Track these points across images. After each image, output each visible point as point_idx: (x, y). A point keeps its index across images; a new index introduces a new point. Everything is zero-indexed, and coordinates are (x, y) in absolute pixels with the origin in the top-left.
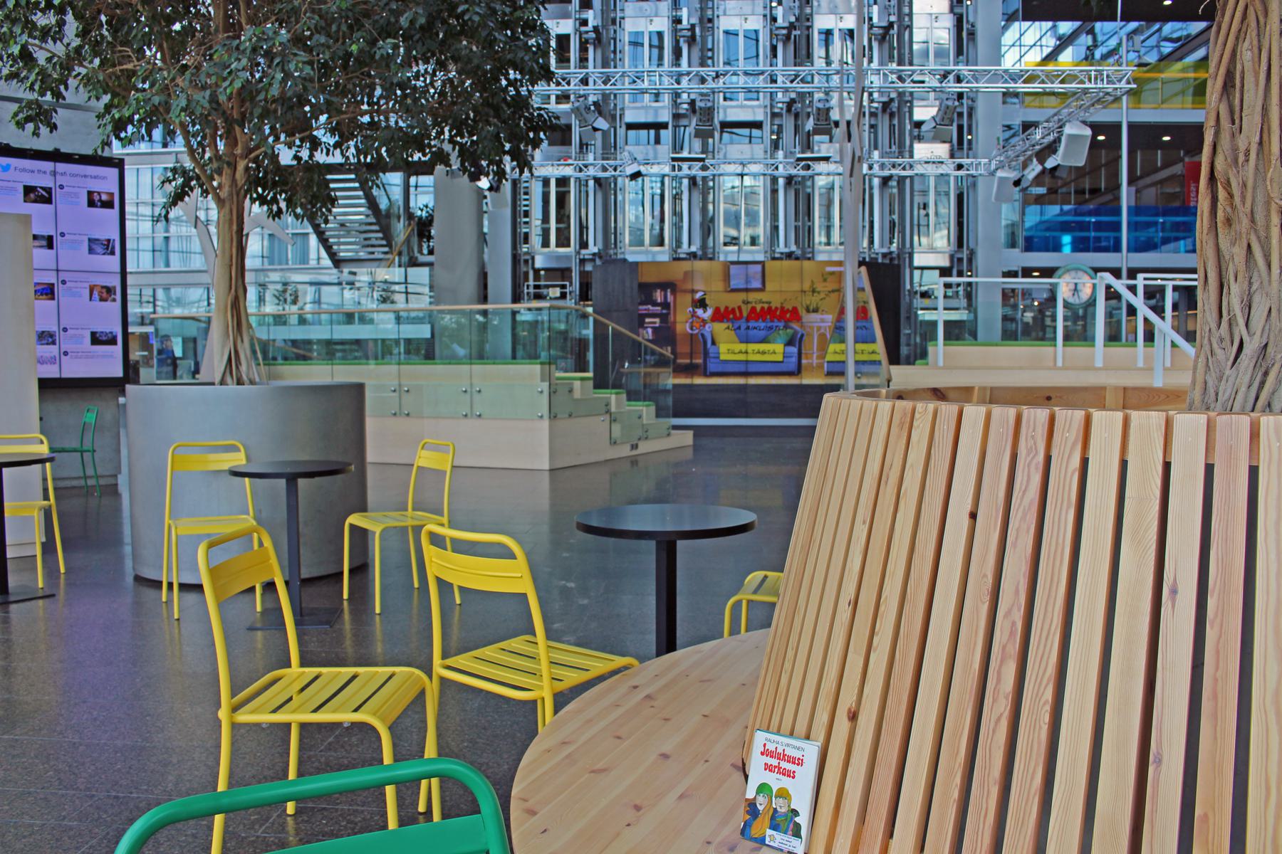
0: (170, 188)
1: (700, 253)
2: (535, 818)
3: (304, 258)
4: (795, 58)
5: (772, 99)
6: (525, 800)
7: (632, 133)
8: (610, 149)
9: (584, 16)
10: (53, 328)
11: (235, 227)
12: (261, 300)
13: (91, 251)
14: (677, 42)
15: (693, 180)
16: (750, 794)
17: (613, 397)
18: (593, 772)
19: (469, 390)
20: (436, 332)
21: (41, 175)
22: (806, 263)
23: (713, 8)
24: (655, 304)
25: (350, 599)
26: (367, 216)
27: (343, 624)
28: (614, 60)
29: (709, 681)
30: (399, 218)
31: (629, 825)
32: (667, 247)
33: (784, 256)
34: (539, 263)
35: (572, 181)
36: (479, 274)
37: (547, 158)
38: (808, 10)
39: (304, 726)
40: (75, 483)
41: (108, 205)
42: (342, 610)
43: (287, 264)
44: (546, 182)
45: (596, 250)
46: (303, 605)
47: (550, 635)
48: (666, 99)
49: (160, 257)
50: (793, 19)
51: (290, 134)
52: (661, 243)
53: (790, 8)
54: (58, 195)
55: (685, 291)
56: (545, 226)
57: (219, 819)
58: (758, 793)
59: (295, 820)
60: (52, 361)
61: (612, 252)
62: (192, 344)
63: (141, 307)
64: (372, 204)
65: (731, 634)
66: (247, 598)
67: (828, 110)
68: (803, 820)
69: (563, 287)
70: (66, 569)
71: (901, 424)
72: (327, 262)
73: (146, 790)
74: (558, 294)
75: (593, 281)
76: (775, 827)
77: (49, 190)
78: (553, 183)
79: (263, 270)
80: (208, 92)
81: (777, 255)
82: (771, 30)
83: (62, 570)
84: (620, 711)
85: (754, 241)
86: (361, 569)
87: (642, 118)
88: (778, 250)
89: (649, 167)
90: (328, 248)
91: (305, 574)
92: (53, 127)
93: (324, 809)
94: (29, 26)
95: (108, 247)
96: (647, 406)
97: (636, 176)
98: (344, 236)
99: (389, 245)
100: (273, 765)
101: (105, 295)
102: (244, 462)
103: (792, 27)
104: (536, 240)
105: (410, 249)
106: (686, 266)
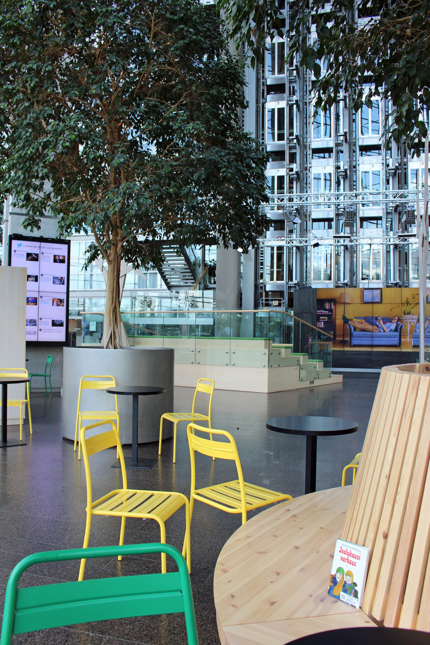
0: (88, 255)
1: (349, 283)
2: (227, 574)
3: (154, 284)
4: (399, 184)
5: (386, 205)
6: (223, 565)
7: (315, 224)
8: (304, 231)
9: (291, 167)
10: (35, 318)
11: (116, 274)
12: (133, 305)
13: (54, 282)
14: (338, 178)
15: (346, 247)
16: (333, 572)
17: (302, 357)
18: (259, 553)
19: (229, 351)
20: (216, 321)
21: (35, 248)
22: (404, 289)
23: (356, 161)
24: (325, 310)
25: (161, 455)
26: (185, 265)
27: (157, 467)
28: (306, 188)
29: (326, 509)
30: (200, 266)
31: (272, 582)
32: (332, 280)
33: (393, 285)
34: (268, 288)
35: (285, 248)
36: (238, 294)
37: (273, 236)
38: (405, 160)
39: (128, 519)
40: (42, 391)
41: (62, 261)
42: (157, 460)
43: (147, 287)
44: (272, 248)
45: (296, 282)
46: (139, 457)
47: (245, 480)
48: (333, 207)
49: (88, 283)
50: (397, 165)
51: (144, 229)
52: (330, 279)
53: (396, 159)
54: (41, 257)
55: (341, 303)
56: (272, 270)
57: (83, 561)
58: (337, 572)
59: (121, 563)
60: (35, 333)
61: (304, 283)
62: (100, 325)
63: (78, 307)
64: (187, 259)
65: (346, 484)
66: (113, 451)
67: (414, 211)
68: (359, 588)
69: (280, 300)
70: (33, 432)
71: (414, 386)
72: (165, 287)
73: (55, 542)
74: (277, 304)
75: (294, 298)
76: (345, 591)
77: (37, 255)
78: (275, 249)
79: (135, 290)
80: (104, 213)
81: (389, 285)
82: (386, 171)
83: (31, 433)
84: (278, 522)
85: (378, 278)
86: (168, 440)
87: (321, 216)
88: (390, 282)
89: (323, 240)
90: (165, 280)
91: (140, 441)
92: (39, 228)
93: (136, 559)
94: (29, 186)
95: (61, 281)
96: (319, 362)
97: (316, 245)
98: (173, 275)
99: (195, 279)
100: (115, 535)
101: (59, 303)
102: (115, 386)
103: (397, 168)
104: (267, 277)
105: (205, 281)
106: (341, 290)
